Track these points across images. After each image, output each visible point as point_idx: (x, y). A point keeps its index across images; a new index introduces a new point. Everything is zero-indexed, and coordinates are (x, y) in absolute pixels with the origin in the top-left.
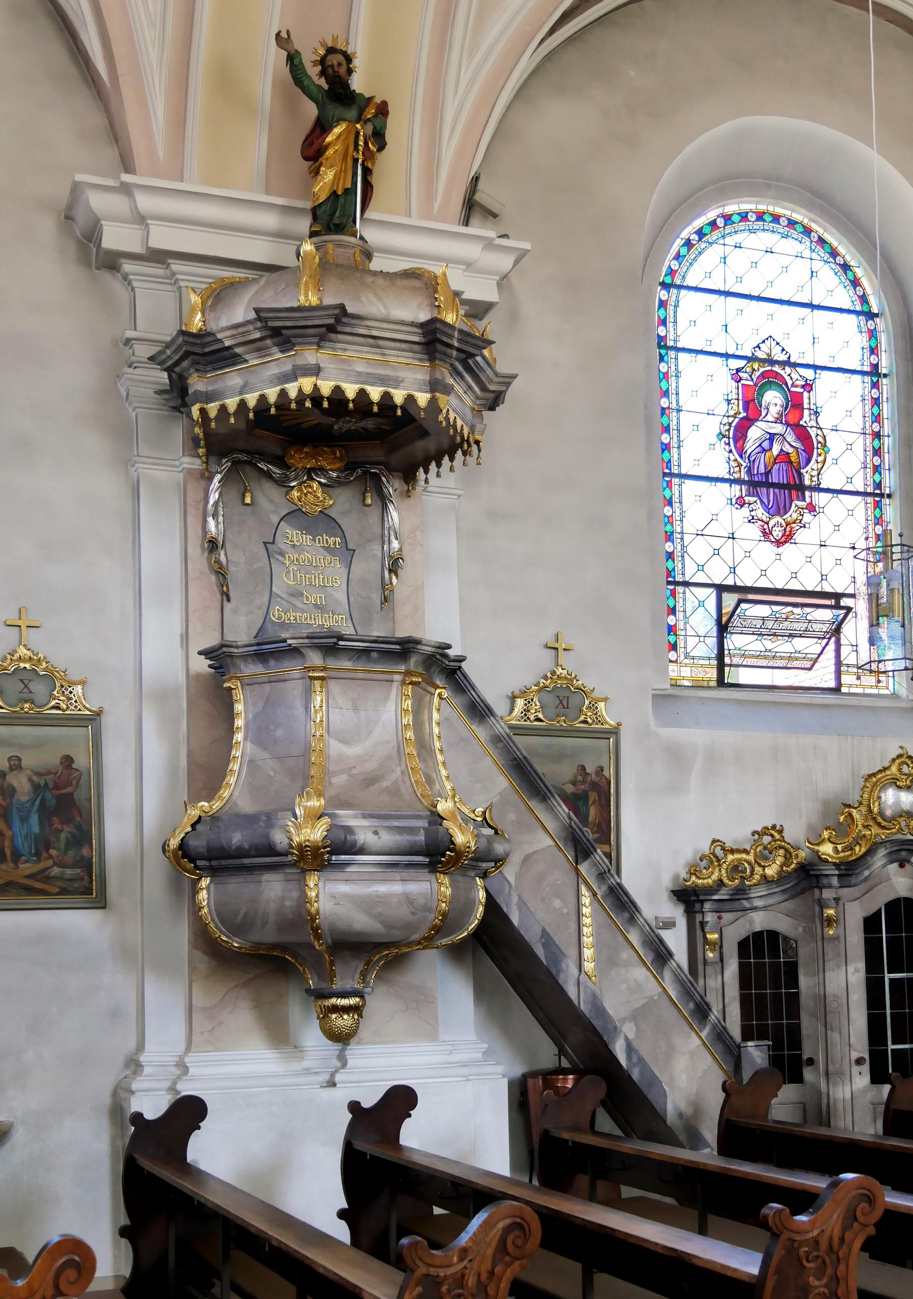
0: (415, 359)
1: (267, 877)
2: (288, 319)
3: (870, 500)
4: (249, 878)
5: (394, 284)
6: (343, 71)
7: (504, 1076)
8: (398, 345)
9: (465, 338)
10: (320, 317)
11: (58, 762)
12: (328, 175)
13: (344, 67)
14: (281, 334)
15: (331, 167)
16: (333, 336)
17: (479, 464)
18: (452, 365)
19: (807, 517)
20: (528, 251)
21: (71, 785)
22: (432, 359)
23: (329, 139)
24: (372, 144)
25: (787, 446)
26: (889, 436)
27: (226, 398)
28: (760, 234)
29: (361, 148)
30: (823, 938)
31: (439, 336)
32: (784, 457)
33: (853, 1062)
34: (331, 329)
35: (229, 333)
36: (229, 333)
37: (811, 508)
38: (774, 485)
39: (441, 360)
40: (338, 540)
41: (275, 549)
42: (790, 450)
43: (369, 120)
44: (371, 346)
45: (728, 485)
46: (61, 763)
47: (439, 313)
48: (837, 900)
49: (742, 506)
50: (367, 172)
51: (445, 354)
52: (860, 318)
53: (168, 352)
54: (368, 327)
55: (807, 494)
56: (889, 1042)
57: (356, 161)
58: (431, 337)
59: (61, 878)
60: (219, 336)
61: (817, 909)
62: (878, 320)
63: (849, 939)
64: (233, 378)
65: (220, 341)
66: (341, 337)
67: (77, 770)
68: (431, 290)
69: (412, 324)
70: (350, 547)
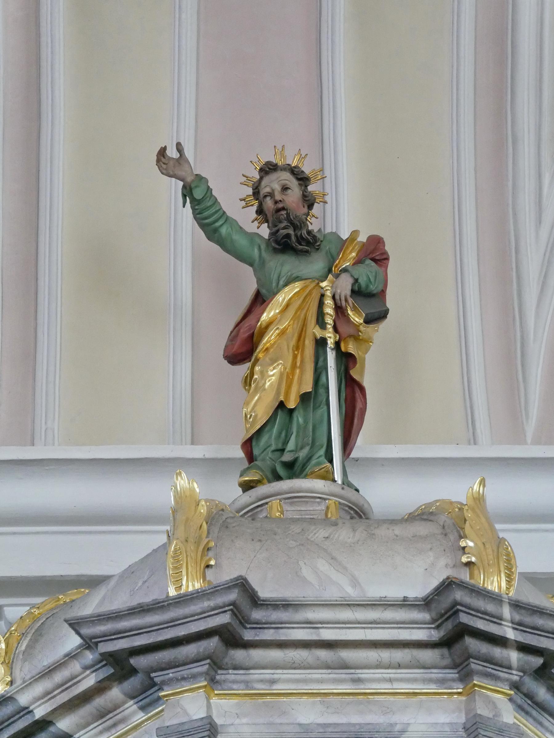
0: (430, 681)
2: (138, 631)
5: (372, 536)
6: (293, 198)
8: (385, 655)
9: (529, 620)
10: (203, 615)
12: (271, 375)
13: (295, 193)
14: (133, 671)
15: (273, 361)
16: (239, 655)
18: (516, 686)
22: (465, 676)
23: (265, 317)
24: (354, 309)
29: (329, 320)
31: (464, 618)
34: (230, 639)
35: (39, 689)
36: (39, 689)
39: (487, 675)
43: (345, 270)
44: (328, 667)
47: (472, 576)
50: (346, 360)
51: (489, 660)
54: (309, 624)
57: (321, 343)
58: (449, 625)
60: (23, 700)
65: (26, 711)
66: (257, 654)
68: (452, 537)
69: (405, 603)
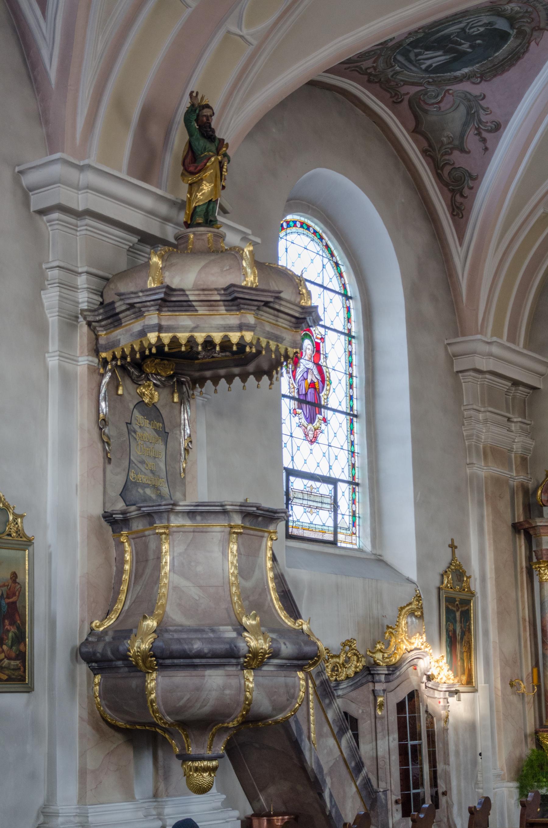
1: (208, 672)
2: (243, 293)
3: (348, 417)
4: (194, 673)
7: (238, 819)
11: (9, 577)
17: (270, 389)
19: (323, 426)
20: (259, 244)
21: (16, 595)
25: (314, 378)
26: (356, 377)
27: (177, 332)
28: (302, 236)
30: (376, 717)
32: (312, 385)
33: (393, 802)
37: (325, 420)
38: (308, 403)
40: (161, 425)
41: (132, 428)
42: (316, 381)
45: (289, 400)
46: (11, 578)
48: (384, 691)
49: (295, 415)
52: (344, 298)
53: (141, 294)
55: (323, 410)
56: (412, 789)
59: (8, 668)
60: (188, 293)
61: (371, 697)
62: (351, 301)
63: (390, 718)
64: (184, 320)
65: (187, 295)
67: (19, 584)
70: (166, 431)
